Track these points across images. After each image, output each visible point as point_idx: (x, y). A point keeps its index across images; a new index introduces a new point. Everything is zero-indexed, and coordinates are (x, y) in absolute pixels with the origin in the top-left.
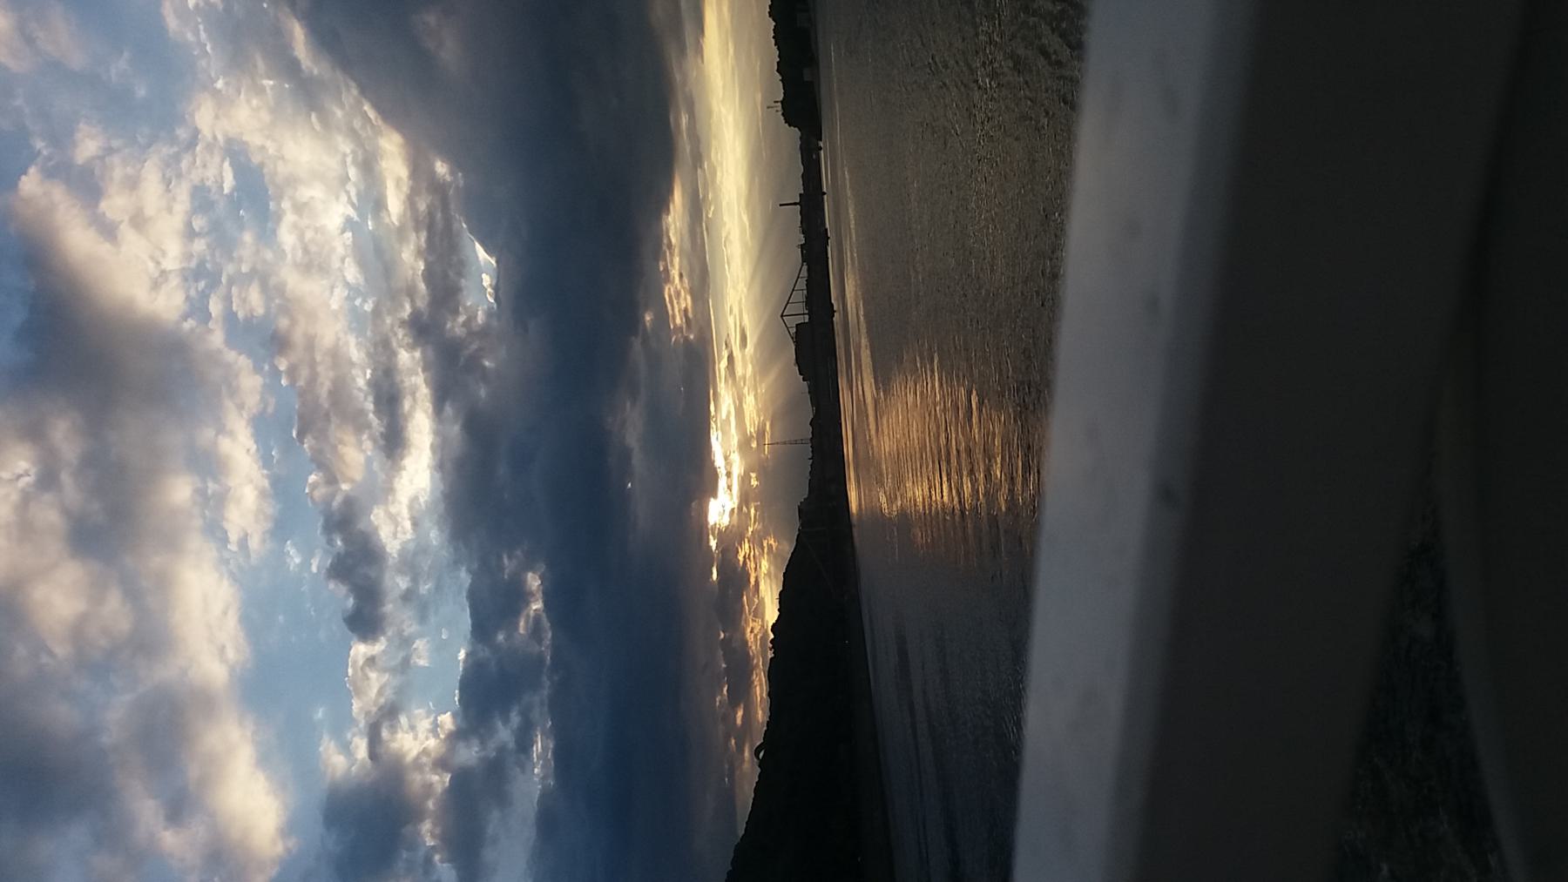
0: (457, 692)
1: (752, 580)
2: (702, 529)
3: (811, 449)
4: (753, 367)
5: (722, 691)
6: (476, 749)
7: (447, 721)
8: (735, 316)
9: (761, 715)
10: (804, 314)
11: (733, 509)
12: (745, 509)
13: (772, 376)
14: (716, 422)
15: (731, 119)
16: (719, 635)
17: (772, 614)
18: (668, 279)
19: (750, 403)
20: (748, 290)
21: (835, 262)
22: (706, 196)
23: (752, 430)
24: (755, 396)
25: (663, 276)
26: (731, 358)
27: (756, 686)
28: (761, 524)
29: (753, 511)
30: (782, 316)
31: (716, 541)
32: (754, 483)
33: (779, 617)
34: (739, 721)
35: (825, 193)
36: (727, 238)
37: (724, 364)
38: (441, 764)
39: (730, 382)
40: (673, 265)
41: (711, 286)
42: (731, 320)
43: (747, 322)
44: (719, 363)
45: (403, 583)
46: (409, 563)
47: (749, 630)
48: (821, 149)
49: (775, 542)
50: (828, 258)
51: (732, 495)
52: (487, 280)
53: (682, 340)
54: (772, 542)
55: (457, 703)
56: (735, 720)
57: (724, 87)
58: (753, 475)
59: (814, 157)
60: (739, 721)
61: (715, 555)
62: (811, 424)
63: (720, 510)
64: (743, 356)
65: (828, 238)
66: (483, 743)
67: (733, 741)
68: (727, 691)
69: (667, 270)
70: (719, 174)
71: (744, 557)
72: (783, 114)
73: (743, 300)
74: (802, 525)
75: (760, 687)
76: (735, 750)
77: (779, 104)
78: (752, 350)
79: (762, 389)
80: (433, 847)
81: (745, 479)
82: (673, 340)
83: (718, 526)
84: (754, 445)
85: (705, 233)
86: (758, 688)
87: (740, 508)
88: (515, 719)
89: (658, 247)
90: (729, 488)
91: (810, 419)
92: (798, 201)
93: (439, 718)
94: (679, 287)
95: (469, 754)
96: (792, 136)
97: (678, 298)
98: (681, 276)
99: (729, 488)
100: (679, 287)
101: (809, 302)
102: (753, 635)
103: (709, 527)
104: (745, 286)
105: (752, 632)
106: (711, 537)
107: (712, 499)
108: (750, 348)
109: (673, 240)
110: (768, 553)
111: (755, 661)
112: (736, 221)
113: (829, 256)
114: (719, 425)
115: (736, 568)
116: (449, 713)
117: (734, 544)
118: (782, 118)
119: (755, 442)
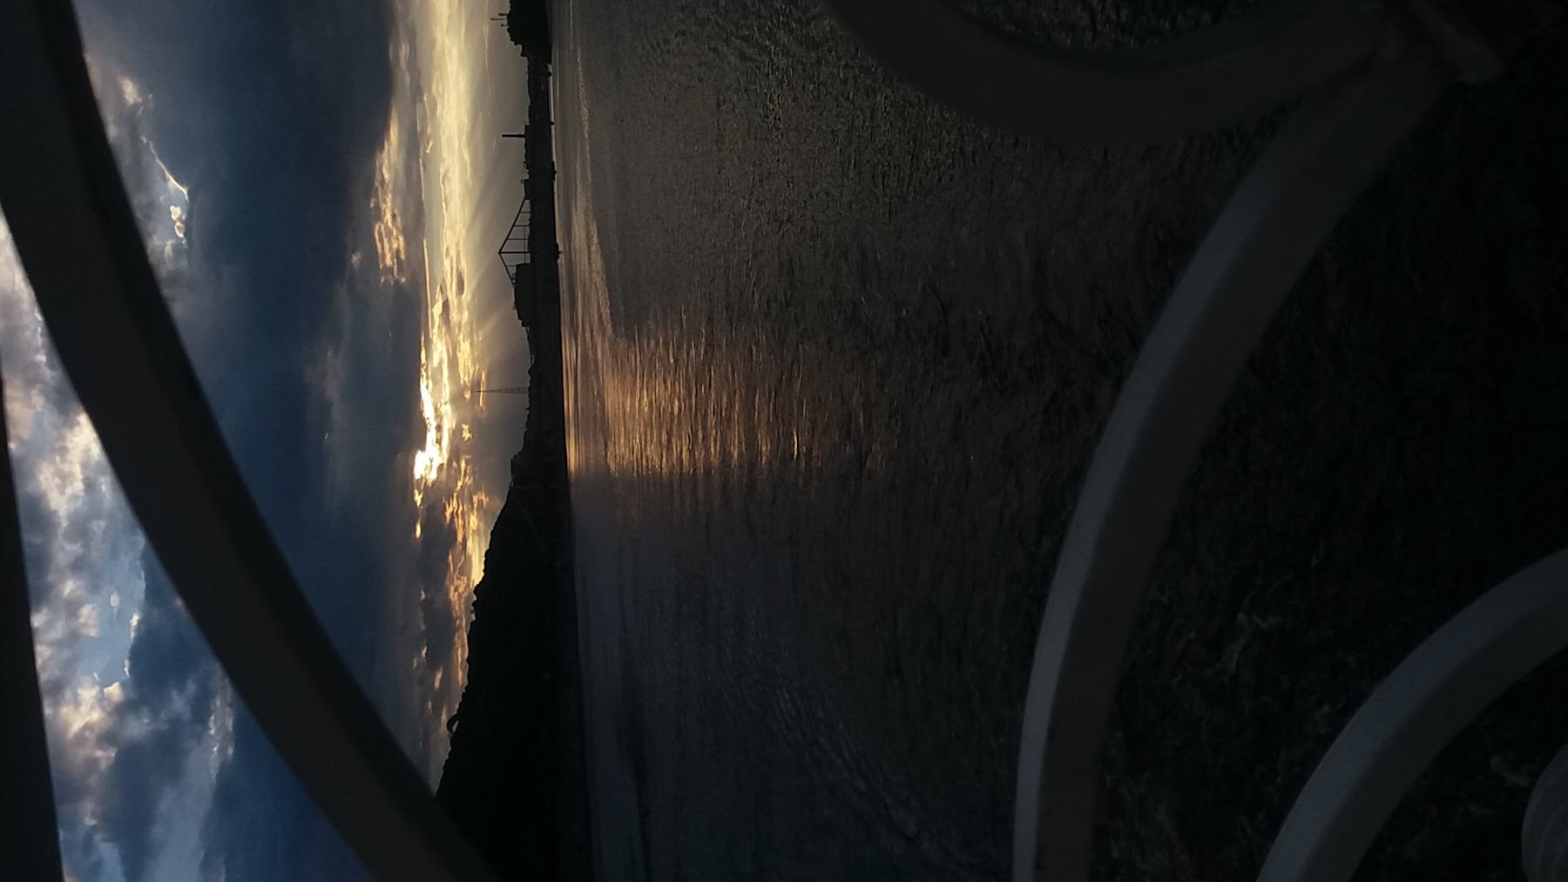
0: (127, 663)
1: (460, 538)
2: (407, 482)
3: (528, 399)
4: (469, 314)
5: (420, 652)
6: (146, 721)
7: (115, 691)
8: (452, 259)
9: (461, 677)
10: (525, 252)
11: (441, 466)
12: (455, 464)
13: (489, 326)
14: (426, 370)
15: (455, 51)
16: (421, 595)
17: (477, 575)
18: (379, 216)
19: (465, 349)
20: (466, 232)
21: (561, 201)
22: (424, 131)
23: (466, 379)
24: (471, 344)
25: (373, 213)
26: (446, 305)
27: (457, 649)
28: (472, 478)
29: (463, 464)
30: (500, 253)
31: (421, 496)
32: (466, 435)
33: (484, 578)
34: (437, 684)
35: (552, 123)
36: (445, 175)
37: (437, 310)
38: (107, 738)
39: (444, 330)
40: (385, 202)
41: (427, 226)
42: (447, 263)
43: (464, 265)
44: (432, 307)
45: (74, 549)
46: (80, 529)
47: (452, 588)
48: (550, 74)
49: (486, 497)
50: (553, 194)
51: (441, 449)
52: (176, 212)
53: (392, 283)
54: (483, 497)
55: (128, 673)
56: (433, 683)
57: (449, 17)
58: (466, 427)
59: (542, 88)
60: (437, 684)
61: (420, 512)
62: (529, 372)
63: (427, 463)
64: (460, 303)
65: (555, 172)
66: (155, 713)
67: (430, 704)
68: (426, 654)
69: (378, 207)
70: (439, 107)
71: (452, 514)
72: (508, 30)
73: (461, 243)
74: (515, 481)
75: (461, 653)
76: (431, 712)
77: (505, 17)
78: (469, 297)
79: (479, 337)
80: (94, 828)
81: (457, 432)
82: (382, 280)
83: (424, 481)
84: (468, 396)
85: (421, 169)
86: (460, 651)
87: (450, 461)
88: (191, 687)
89: (369, 186)
90: (439, 441)
91: (517, 315)
92: (523, 133)
93: (105, 690)
94: (390, 224)
95: (139, 727)
96: (515, 60)
97: (390, 243)
98: (394, 216)
99: (439, 441)
100: (390, 224)
101: (532, 241)
102: (456, 594)
103: (415, 481)
104: (464, 226)
105: (456, 590)
106: (416, 492)
107: (419, 452)
108: (467, 295)
109: (386, 176)
110: (477, 510)
111: (458, 622)
112: (456, 159)
113: (556, 191)
114: (430, 373)
115: (443, 526)
116: (117, 684)
117: (442, 500)
118: (508, 34)
119: (469, 393)
